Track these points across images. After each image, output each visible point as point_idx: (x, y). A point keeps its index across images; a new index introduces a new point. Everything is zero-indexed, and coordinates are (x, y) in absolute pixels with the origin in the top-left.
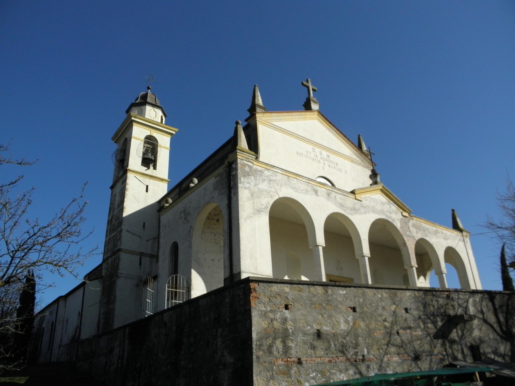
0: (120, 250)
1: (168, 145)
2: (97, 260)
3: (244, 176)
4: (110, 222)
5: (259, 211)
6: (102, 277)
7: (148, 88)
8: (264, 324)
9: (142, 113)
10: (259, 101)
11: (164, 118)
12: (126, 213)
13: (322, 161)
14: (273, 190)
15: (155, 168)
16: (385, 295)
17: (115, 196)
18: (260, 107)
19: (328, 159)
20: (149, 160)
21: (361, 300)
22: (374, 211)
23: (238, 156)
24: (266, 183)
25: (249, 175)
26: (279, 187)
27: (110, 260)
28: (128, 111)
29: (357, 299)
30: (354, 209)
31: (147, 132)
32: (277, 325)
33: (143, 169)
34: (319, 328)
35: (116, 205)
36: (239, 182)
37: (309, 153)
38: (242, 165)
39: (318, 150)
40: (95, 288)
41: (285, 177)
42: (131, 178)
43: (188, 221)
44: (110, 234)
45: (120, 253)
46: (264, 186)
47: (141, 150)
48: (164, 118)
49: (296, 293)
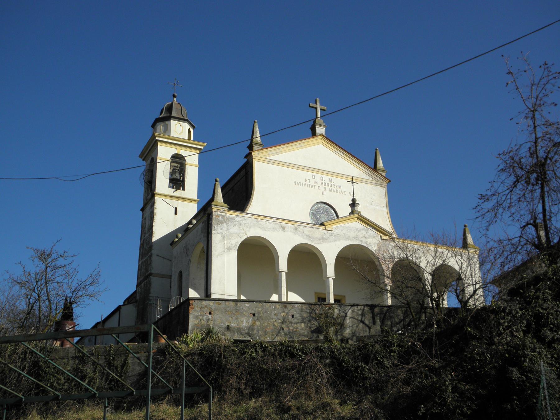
0: (151, 274)
1: (197, 162)
2: (129, 286)
3: (218, 224)
4: (142, 246)
5: (229, 249)
6: (136, 302)
7: (174, 96)
8: (196, 322)
9: (167, 130)
10: (258, 138)
11: (192, 130)
12: (156, 237)
13: (322, 187)
14: (242, 232)
15: (183, 189)
16: (278, 306)
17: (145, 219)
18: (258, 144)
19: (330, 183)
20: (177, 182)
21: (260, 310)
22: (345, 238)
23: (213, 210)
24: (237, 227)
25: (221, 223)
26: (248, 229)
27: (143, 284)
28: (154, 126)
29: (257, 309)
30: (323, 239)
31: (173, 150)
32: (203, 322)
33: (171, 192)
34: (229, 324)
35: (146, 229)
36: (213, 229)
37: (308, 181)
38: (216, 216)
39: (318, 176)
40: (131, 311)
41: (254, 220)
42: (158, 200)
43: (188, 255)
44: (142, 258)
45: (151, 277)
46: (234, 229)
47: (168, 170)
48: (192, 130)
49: (217, 305)
